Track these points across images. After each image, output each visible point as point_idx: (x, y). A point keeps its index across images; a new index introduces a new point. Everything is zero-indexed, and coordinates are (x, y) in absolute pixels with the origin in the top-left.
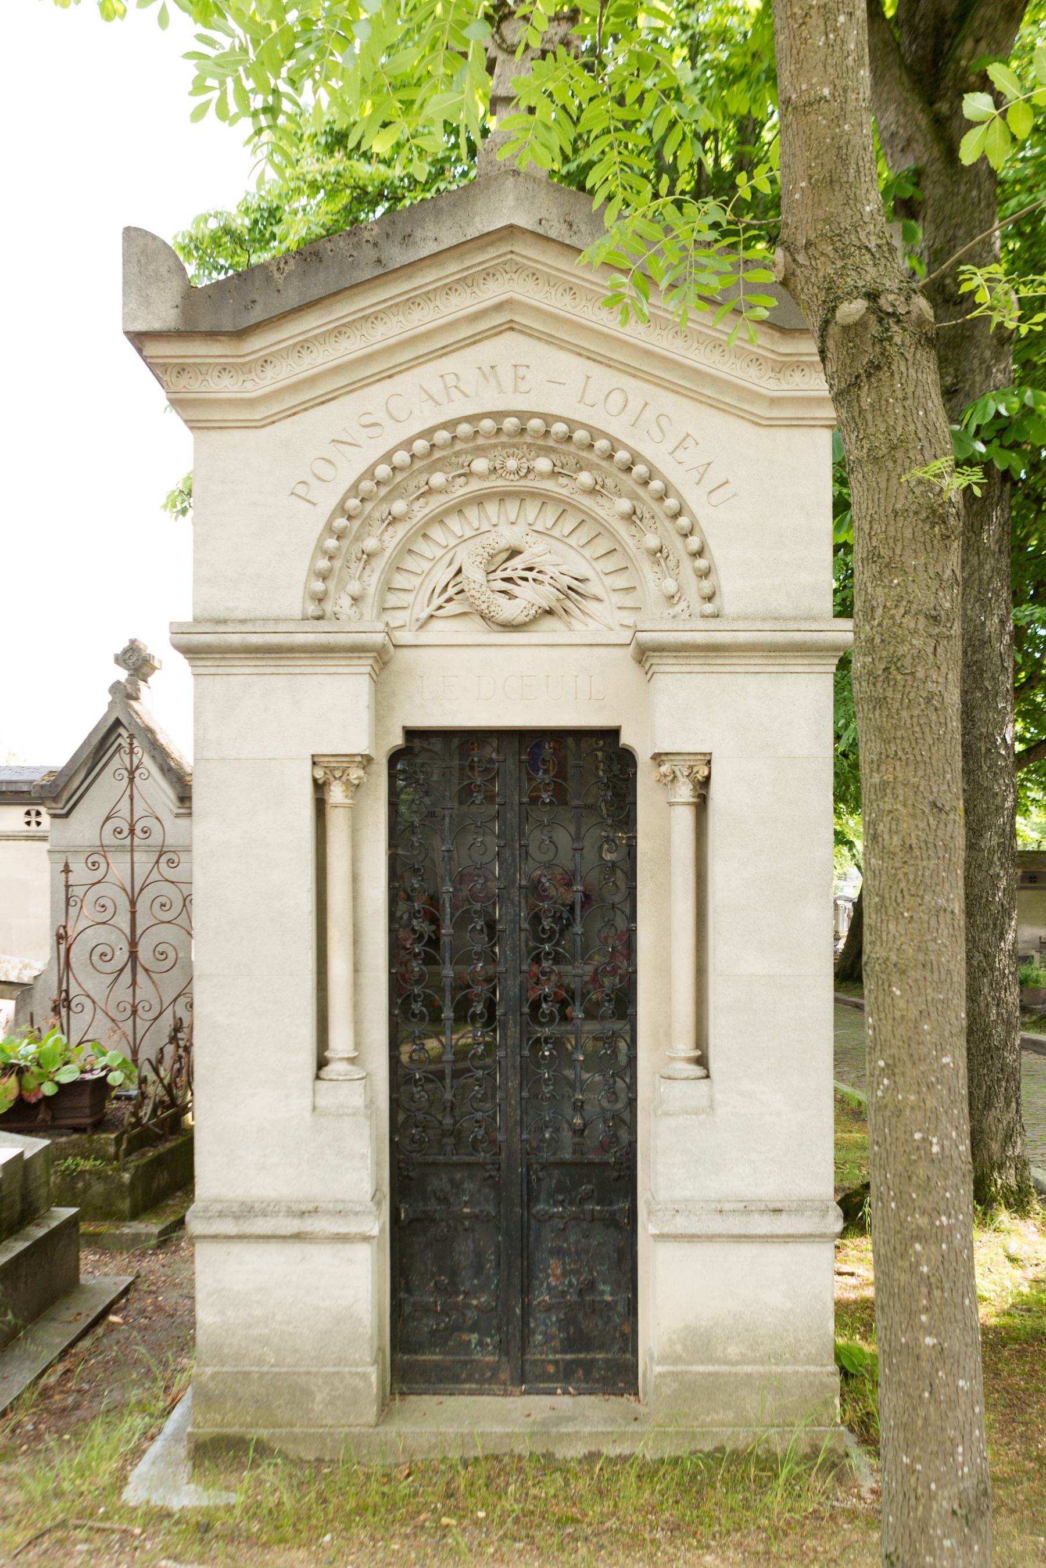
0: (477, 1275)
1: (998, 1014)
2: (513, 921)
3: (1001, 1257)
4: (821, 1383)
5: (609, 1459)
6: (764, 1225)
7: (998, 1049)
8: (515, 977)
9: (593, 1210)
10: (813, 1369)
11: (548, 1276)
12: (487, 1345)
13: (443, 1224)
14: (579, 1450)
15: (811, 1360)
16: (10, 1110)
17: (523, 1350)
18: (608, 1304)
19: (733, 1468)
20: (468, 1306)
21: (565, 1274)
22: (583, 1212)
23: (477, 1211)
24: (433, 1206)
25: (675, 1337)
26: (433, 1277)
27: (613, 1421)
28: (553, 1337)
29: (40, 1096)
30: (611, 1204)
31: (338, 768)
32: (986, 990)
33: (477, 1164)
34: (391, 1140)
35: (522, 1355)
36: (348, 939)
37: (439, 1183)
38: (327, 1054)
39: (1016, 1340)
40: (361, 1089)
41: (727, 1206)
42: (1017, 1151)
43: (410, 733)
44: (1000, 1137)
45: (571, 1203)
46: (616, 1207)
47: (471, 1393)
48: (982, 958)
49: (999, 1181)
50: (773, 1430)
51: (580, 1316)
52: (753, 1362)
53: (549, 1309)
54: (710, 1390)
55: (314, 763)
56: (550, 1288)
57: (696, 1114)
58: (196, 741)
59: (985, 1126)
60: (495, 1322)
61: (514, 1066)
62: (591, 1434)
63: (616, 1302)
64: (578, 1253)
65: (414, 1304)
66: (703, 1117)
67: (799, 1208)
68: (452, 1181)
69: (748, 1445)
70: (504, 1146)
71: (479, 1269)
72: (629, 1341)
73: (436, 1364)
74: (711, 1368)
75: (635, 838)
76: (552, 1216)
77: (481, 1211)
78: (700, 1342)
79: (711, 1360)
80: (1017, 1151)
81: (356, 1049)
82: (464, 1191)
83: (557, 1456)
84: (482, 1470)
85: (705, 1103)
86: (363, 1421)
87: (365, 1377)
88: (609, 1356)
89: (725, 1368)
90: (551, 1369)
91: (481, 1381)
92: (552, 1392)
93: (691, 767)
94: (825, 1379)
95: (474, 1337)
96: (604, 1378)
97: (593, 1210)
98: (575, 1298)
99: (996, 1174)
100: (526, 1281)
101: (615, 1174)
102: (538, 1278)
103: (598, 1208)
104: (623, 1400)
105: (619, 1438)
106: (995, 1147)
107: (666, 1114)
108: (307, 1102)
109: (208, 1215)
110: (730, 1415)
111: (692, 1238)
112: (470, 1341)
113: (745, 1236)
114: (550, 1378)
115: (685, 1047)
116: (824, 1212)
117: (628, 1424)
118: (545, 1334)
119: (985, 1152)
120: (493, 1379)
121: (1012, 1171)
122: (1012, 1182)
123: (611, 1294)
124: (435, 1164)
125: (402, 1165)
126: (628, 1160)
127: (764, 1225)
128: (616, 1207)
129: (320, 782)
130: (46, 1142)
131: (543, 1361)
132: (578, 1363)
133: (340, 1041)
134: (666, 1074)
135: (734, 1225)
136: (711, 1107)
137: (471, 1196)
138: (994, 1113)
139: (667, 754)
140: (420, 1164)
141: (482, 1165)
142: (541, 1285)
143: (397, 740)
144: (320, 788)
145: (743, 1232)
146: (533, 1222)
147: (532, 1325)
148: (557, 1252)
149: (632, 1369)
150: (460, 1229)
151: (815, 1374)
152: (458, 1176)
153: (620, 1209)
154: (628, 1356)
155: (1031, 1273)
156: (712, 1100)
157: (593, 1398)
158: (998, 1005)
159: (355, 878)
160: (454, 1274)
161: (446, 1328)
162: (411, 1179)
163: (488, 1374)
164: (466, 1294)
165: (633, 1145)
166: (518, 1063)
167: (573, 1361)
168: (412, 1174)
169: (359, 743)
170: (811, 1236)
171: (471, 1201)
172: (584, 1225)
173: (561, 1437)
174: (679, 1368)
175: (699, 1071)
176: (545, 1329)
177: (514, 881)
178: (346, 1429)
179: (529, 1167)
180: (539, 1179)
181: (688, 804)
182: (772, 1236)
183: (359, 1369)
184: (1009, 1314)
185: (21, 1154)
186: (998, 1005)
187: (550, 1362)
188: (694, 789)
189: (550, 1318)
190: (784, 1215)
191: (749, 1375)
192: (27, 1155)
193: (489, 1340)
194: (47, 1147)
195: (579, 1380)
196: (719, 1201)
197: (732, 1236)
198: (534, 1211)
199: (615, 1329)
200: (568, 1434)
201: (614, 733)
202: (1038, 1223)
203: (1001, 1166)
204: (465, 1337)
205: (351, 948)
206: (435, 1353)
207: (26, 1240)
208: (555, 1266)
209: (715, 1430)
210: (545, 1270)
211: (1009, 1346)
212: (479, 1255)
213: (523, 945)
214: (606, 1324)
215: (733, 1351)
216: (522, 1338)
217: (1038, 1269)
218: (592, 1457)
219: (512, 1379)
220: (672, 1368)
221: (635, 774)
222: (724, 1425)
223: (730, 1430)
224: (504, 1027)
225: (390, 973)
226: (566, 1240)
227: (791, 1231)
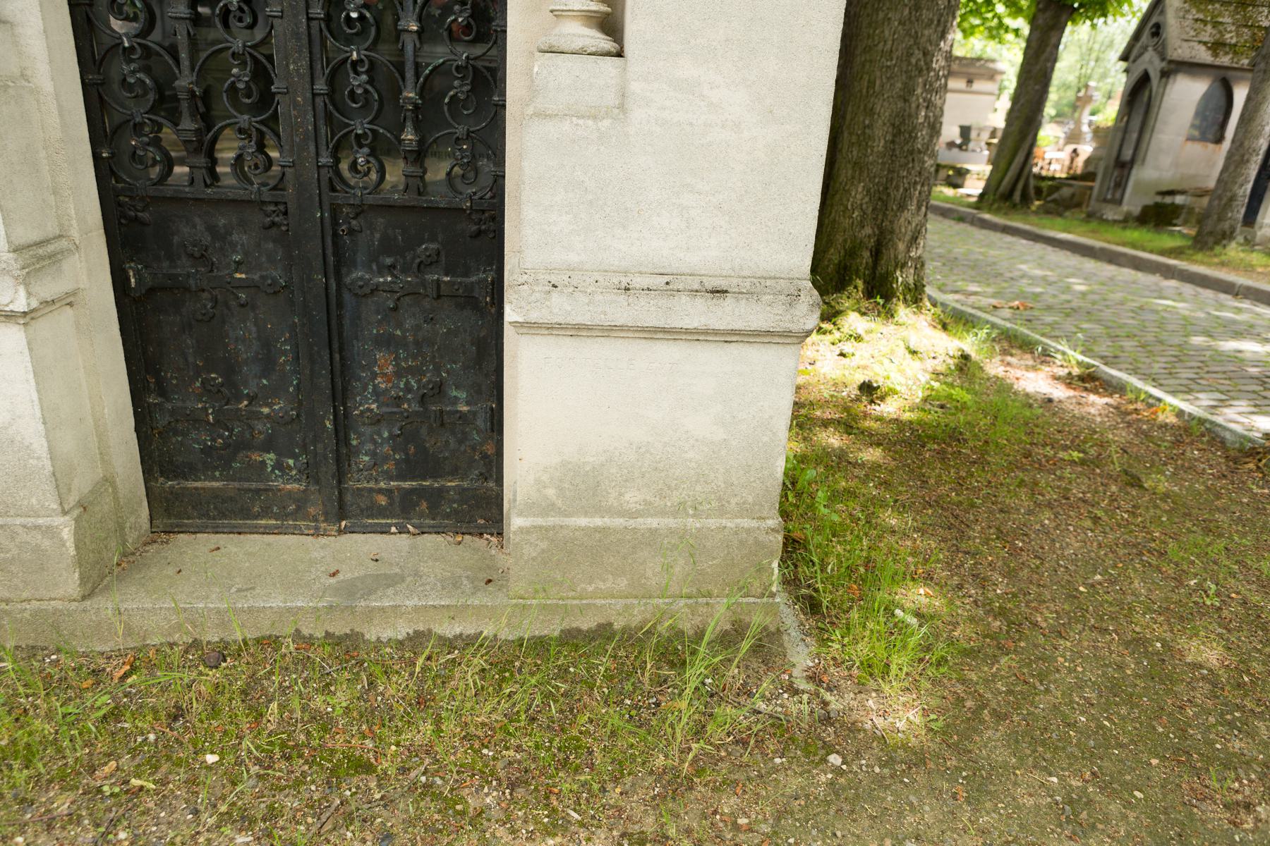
0: (266, 373)
1: (926, 117)
3: (901, 350)
4: (757, 542)
5: (442, 640)
6: (696, 313)
7: (920, 152)
9: (438, 282)
10: (746, 523)
11: (375, 376)
12: (291, 469)
13: (205, 295)
14: (402, 630)
15: (744, 511)
17: (340, 476)
18: (462, 416)
19: (622, 653)
20: (258, 416)
21: (399, 374)
22: (423, 284)
23: (256, 277)
24: (184, 267)
25: (545, 478)
26: (198, 374)
27: (456, 584)
28: (386, 458)
30: (466, 274)
32: (919, 91)
34: (96, 157)
35: (340, 482)
39: (934, 439)
41: (638, 282)
42: (919, 252)
44: (908, 238)
45: (405, 271)
46: (474, 279)
47: (267, 531)
48: (921, 56)
49: (900, 279)
50: (683, 602)
51: (424, 431)
52: (662, 513)
53: (377, 420)
54: (598, 547)
56: (377, 393)
57: (595, 118)
59: (896, 227)
60: (298, 438)
61: (296, 35)
62: (416, 609)
63: (474, 414)
64: (417, 343)
65: (173, 412)
67: (754, 288)
68: (211, 229)
69: (645, 622)
71: (267, 363)
72: (492, 465)
73: (215, 494)
74: (598, 521)
76: (375, 290)
78: (584, 486)
79: (599, 510)
80: (919, 252)
82: (233, 245)
83: (367, 637)
84: (238, 670)
85: (611, 99)
86: (60, 592)
87: (50, 531)
88: (465, 484)
89: (619, 522)
90: (382, 500)
91: (283, 516)
92: (384, 531)
94: (762, 537)
95: (270, 458)
96: (456, 512)
97: (438, 282)
98: (415, 407)
99: (898, 273)
100: (339, 381)
102: (359, 379)
104: (480, 543)
105: (454, 613)
106: (901, 246)
107: (543, 115)
109: (1057, 333)
110: (623, 583)
111: (577, 330)
112: (263, 463)
113: (664, 330)
114: (382, 512)
116: (795, 296)
117: (476, 590)
118: (373, 454)
119: (892, 251)
120: (300, 512)
121: (912, 271)
122: (911, 280)
123: (468, 403)
127: (696, 313)
128: (474, 279)
131: (371, 490)
132: (420, 493)
135: (649, 312)
136: (622, 107)
137: (246, 254)
138: (906, 215)
142: (365, 388)
145: (661, 324)
146: (347, 296)
147: (354, 443)
148: (386, 342)
149: (496, 501)
150: (233, 303)
151: (748, 531)
152: (222, 222)
153: (479, 282)
154: (491, 484)
155: (930, 365)
157: (439, 538)
158: (927, 107)
160: (230, 370)
161: (226, 446)
162: (143, 224)
163: (293, 507)
164: (252, 399)
165: (499, 179)
167: (412, 491)
168: (145, 216)
170: (768, 333)
171: (247, 259)
172: (426, 303)
173: (370, 614)
174: (551, 521)
175: (606, 44)
176: (372, 449)
178: (35, 604)
179: (335, 211)
182: (706, 332)
183: (40, 521)
184: (923, 410)
186: (927, 107)
187: (380, 491)
189: (380, 435)
190: (729, 299)
191: (653, 532)
193: (291, 462)
195: (421, 515)
196: (626, 273)
197: (643, 329)
198: (348, 280)
199: (474, 449)
200: (383, 609)
202: (929, 318)
203: (904, 265)
204: (256, 457)
206: (214, 479)
208: (385, 362)
209: (599, 602)
210: (369, 367)
211: (928, 446)
212: (267, 344)
214: (460, 442)
215: (633, 498)
216: (338, 461)
217: (936, 362)
218: (417, 640)
219: (326, 514)
220: (540, 521)
222: (613, 597)
223: (622, 601)
226: (400, 325)
227: (738, 325)
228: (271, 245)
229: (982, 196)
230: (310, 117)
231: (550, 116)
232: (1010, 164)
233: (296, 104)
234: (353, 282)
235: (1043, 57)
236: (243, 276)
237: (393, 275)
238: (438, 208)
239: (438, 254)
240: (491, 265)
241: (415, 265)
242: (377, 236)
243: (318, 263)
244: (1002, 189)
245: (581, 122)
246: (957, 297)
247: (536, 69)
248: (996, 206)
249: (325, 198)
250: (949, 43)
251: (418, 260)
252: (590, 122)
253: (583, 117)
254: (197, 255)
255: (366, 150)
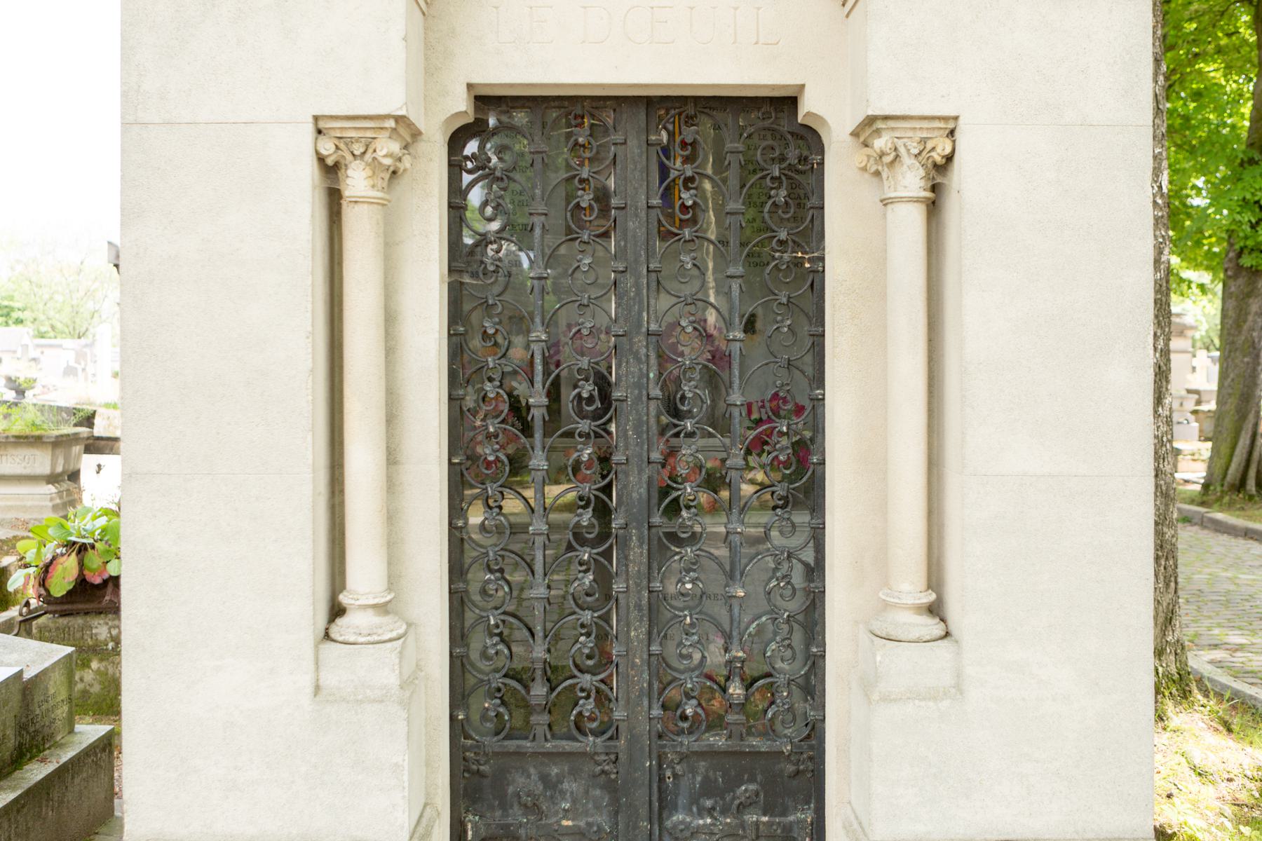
2: (638, 385)
8: (640, 471)
16: (70, 593)
22: (742, 825)
23: (582, 824)
24: (517, 817)
29: (106, 576)
30: (784, 813)
31: (358, 140)
33: (584, 754)
34: (452, 718)
36: (379, 415)
37: (524, 782)
38: (344, 599)
40: (394, 658)
43: (484, 101)
45: (725, 812)
46: (792, 818)
55: (319, 132)
58: (124, 95)
61: (639, 607)
66: (946, 703)
68: (544, 778)
70: (623, 726)
75: (822, 259)
77: (589, 825)
81: (389, 589)
82: (562, 793)
93: (924, 141)
97: (757, 824)
101: (791, 768)
103: (765, 819)
107: (886, 699)
108: (307, 681)
115: (910, 587)
121: (1172, 657)
122: (1173, 670)
124: (519, 754)
125: (469, 755)
126: (811, 748)
128: (792, 818)
129: (330, 162)
130: (70, 649)
133: (365, 577)
134: (877, 626)
136: (958, 689)
137: (574, 802)
139: (886, 118)
140: (496, 754)
141: (592, 756)
143: (460, 105)
144: (331, 170)
152: (555, 771)
156: (959, 675)
159: (390, 319)
166: (645, 602)
169: (388, 94)
175: (936, 628)
177: (639, 325)
179: (661, 759)
180: (675, 776)
181: (917, 200)
185: (21, 672)
188: (927, 177)
192: (27, 676)
194: (69, 656)
198: (668, 824)
201: (787, 103)
205: (382, 428)
207: (14, 789)
213: (652, 421)
221: (822, 164)
224: (624, 544)
225: (450, 463)
228: (598, 792)
229: (1206, 486)
230: (646, 676)
231: (895, 700)
232: (1231, 455)
233: (634, 665)
234: (675, 826)
235: (1245, 327)
236: (570, 823)
237: (712, 817)
238: (760, 753)
239: (757, 795)
240: (808, 803)
241: (734, 807)
242: (699, 779)
243: (643, 811)
244: (1229, 478)
245: (923, 703)
246: (1218, 655)
247: (878, 658)
248: (1226, 499)
249: (654, 747)
250: (1167, 407)
251: (737, 802)
252: (931, 704)
253: (924, 699)
254: (529, 804)
255: (694, 702)
